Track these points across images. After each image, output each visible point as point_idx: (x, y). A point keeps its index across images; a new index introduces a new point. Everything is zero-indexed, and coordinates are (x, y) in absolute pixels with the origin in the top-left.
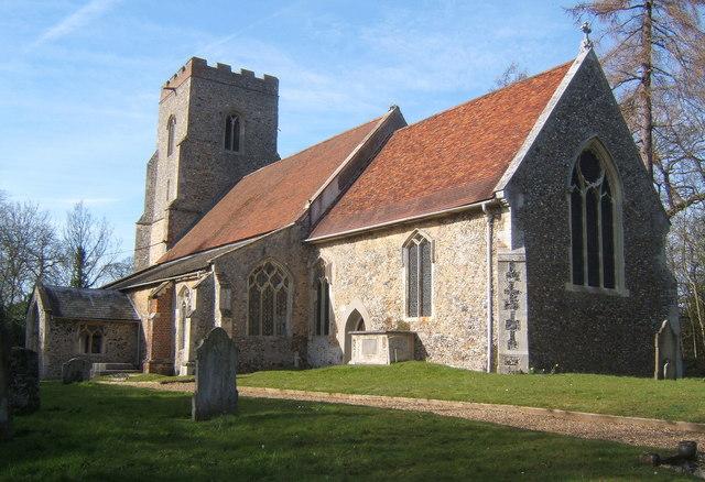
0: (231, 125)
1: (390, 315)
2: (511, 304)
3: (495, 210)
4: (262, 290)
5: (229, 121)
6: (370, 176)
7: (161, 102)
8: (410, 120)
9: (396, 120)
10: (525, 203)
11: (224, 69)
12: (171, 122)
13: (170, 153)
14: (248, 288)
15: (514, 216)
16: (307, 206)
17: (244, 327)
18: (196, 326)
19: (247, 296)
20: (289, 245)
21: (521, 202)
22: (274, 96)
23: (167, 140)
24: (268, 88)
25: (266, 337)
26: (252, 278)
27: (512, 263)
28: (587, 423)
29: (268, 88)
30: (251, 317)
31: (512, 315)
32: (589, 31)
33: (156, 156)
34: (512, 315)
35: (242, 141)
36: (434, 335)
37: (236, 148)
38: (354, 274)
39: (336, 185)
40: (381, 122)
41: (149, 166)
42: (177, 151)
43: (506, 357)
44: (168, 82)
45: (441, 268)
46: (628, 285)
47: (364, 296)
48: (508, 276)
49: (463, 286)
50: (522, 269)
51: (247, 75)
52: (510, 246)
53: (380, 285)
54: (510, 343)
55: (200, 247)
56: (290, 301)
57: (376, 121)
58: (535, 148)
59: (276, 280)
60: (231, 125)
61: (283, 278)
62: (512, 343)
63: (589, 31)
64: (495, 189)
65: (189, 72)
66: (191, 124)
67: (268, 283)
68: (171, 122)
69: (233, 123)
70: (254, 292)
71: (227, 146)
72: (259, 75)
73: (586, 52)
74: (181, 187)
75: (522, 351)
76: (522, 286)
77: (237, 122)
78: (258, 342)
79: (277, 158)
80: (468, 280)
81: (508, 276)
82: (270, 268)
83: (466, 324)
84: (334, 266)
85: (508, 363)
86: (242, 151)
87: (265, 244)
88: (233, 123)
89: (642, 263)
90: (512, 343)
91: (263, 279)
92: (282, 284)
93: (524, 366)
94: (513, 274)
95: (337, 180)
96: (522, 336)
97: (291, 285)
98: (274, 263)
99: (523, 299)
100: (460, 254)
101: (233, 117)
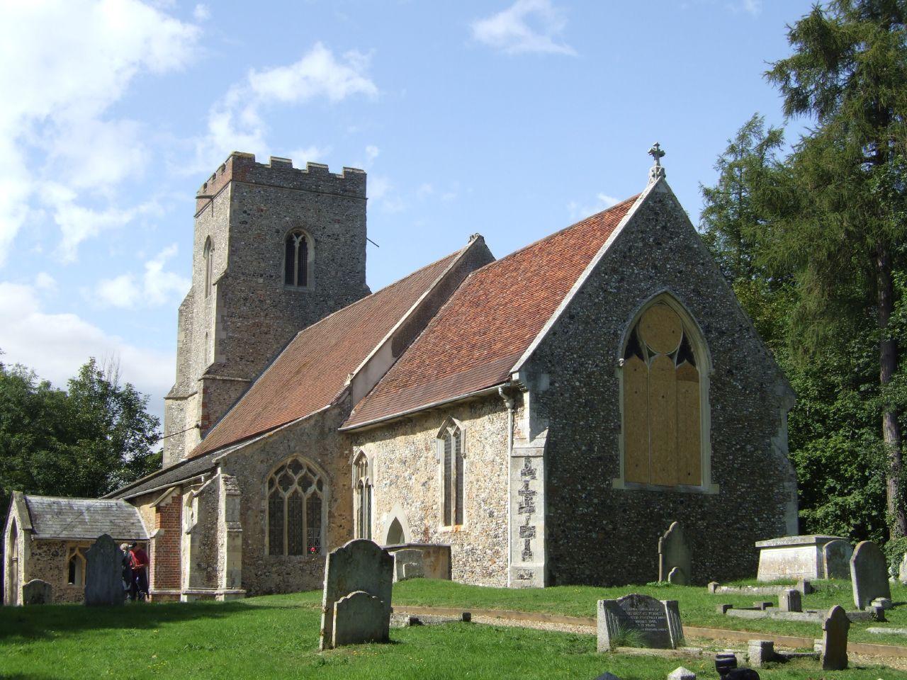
0: (293, 250)
1: (428, 524)
2: (527, 507)
3: (514, 394)
4: (286, 495)
5: (290, 242)
6: (425, 339)
7: (197, 216)
8: (499, 249)
9: (478, 254)
10: (552, 384)
11: (281, 167)
12: (209, 245)
13: (207, 294)
14: (267, 494)
15: (534, 401)
16: (348, 383)
17: (264, 545)
18: (197, 544)
19: (265, 505)
20: (323, 435)
21: (544, 382)
22: (360, 199)
23: (204, 273)
24: (353, 185)
25: (293, 557)
26: (271, 483)
27: (528, 457)
28: (22, 596)
29: (353, 185)
30: (271, 532)
31: (528, 520)
32: (662, 154)
33: (191, 296)
34: (528, 520)
35: (311, 270)
36: (467, 547)
37: (302, 282)
38: (395, 473)
39: (389, 350)
40: (459, 256)
41: (180, 311)
42: (214, 289)
43: (518, 569)
44: (205, 186)
45: (472, 463)
46: (716, 479)
47: (406, 501)
48: (523, 474)
49: (490, 486)
50: (539, 465)
51: (317, 172)
52: (528, 439)
53: (419, 487)
54: (525, 554)
55: (343, 407)
56: (325, 509)
57: (455, 255)
58: (569, 314)
59: (305, 483)
60: (293, 250)
61: (315, 480)
62: (527, 553)
63: (662, 154)
64: (511, 371)
65: (229, 174)
66: (233, 251)
67: (296, 486)
68: (209, 245)
69: (297, 245)
70: (276, 502)
71: (289, 280)
72: (336, 169)
73: (655, 181)
74: (220, 343)
75: (538, 563)
76: (538, 485)
77: (303, 244)
78: (281, 563)
79: (367, 291)
80: (495, 479)
81: (523, 474)
82: (296, 466)
83: (492, 533)
84: (375, 462)
85: (522, 577)
86: (311, 286)
87: (292, 432)
88: (297, 245)
89: (743, 448)
90: (527, 553)
91: (286, 482)
92: (314, 487)
93: (539, 581)
94: (529, 472)
95: (390, 344)
96: (538, 544)
97: (326, 488)
98: (302, 460)
99: (539, 502)
100: (488, 447)
101: (298, 235)
